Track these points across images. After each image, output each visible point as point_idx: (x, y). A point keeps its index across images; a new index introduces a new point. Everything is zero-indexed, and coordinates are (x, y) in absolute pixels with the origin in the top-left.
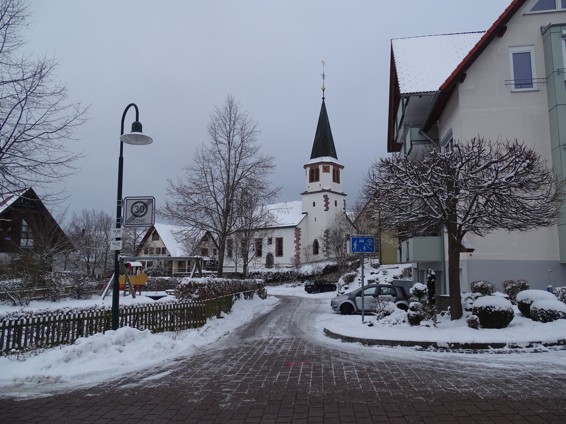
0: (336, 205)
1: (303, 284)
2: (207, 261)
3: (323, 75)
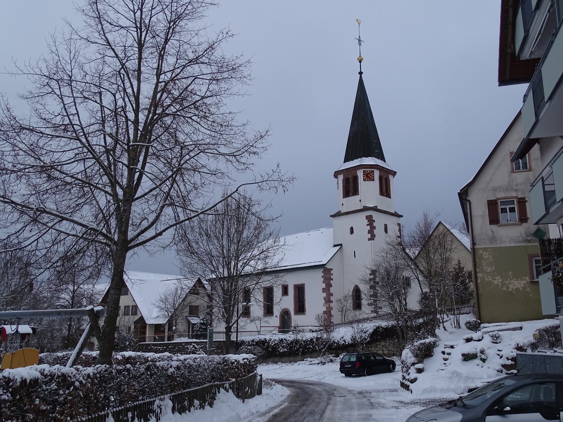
0: (386, 231)
1: (338, 358)
2: (195, 324)
3: (359, 40)
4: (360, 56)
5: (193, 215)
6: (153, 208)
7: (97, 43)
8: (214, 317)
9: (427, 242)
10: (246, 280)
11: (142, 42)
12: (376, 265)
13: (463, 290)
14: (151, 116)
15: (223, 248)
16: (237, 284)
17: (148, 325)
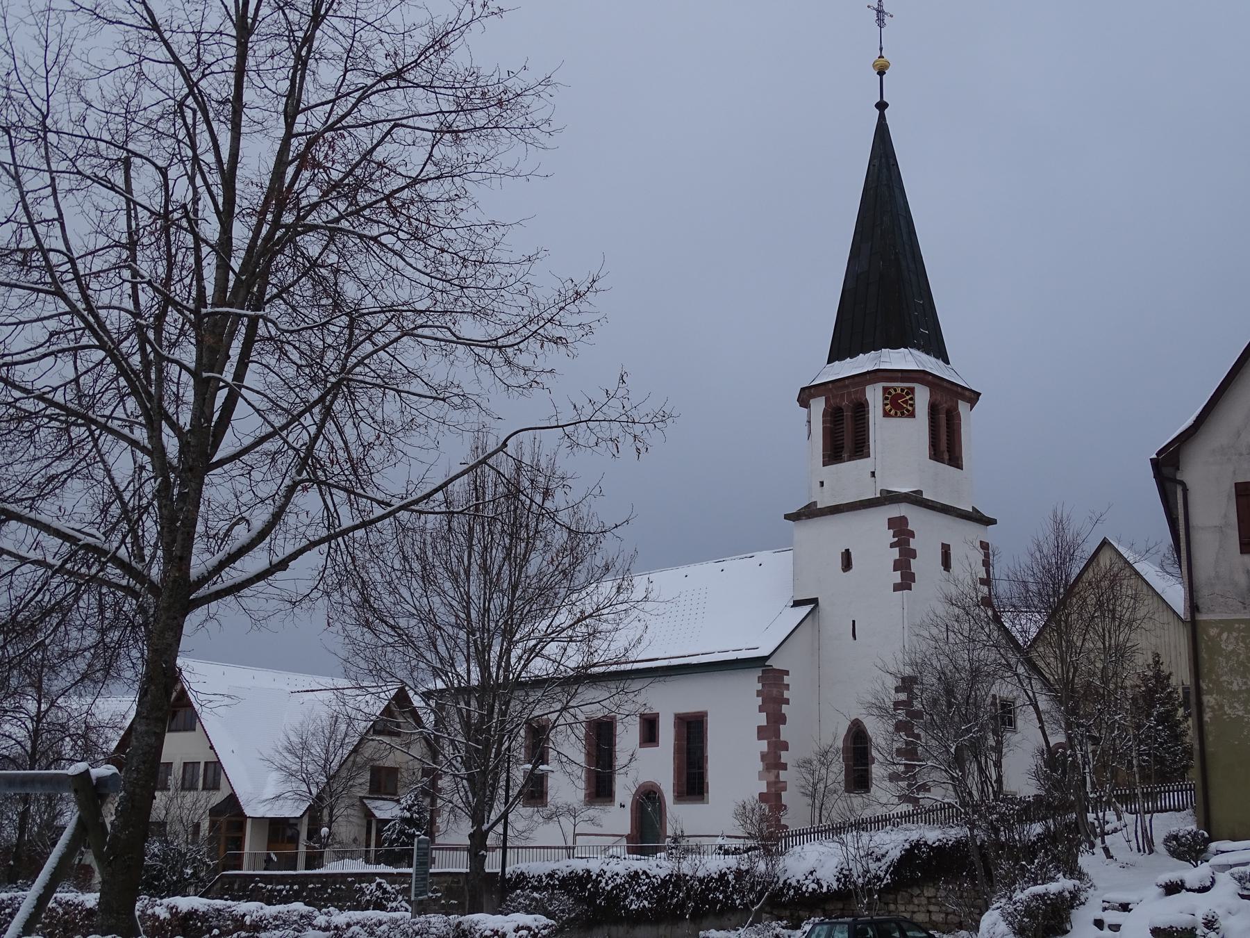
0: (946, 564)
1: (799, 932)
2: (388, 821)
3: (880, 12)
4: (881, 57)
5: (379, 511)
6: (265, 490)
7: (121, 23)
8: (439, 802)
9: (1063, 603)
10: (531, 700)
11: (250, 21)
12: (913, 664)
13: (1166, 742)
14: (265, 229)
15: (468, 603)
16: (507, 708)
17: (249, 821)
